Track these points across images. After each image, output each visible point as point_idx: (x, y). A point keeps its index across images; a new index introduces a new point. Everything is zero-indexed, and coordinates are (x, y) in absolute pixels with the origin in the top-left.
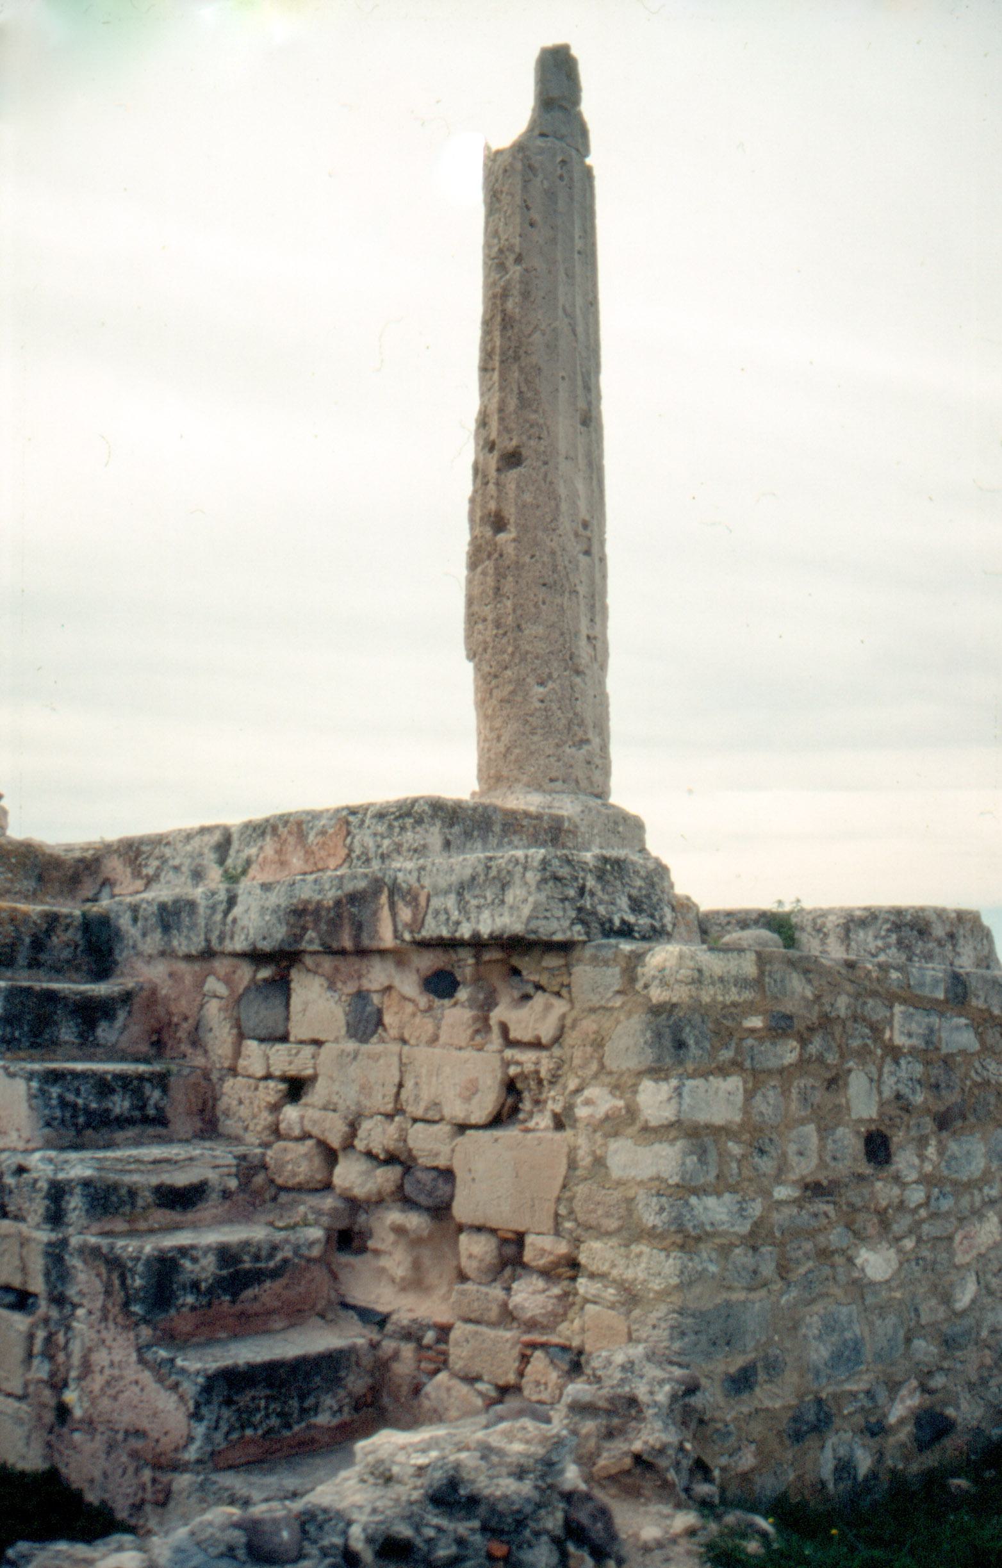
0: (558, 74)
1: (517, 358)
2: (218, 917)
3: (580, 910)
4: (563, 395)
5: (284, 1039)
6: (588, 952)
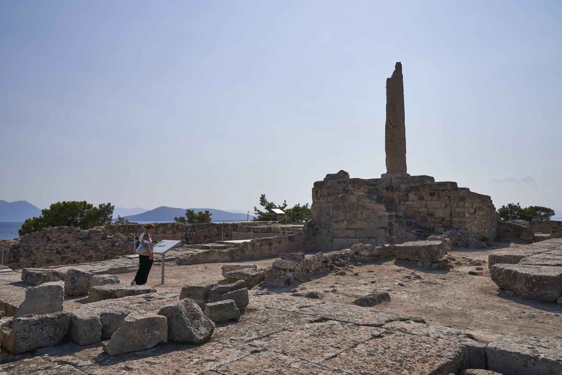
0: (399, 66)
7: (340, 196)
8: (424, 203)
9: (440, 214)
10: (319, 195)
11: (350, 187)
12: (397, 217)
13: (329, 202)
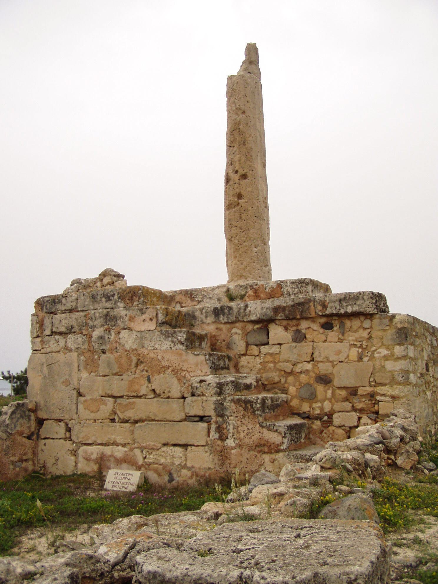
0: (252, 53)
1: (244, 145)
2: (242, 311)
3: (377, 306)
4: (259, 158)
5: (267, 344)
6: (377, 316)
7: (97, 333)
8: (306, 348)
9: (344, 377)
10: (48, 332)
11: (121, 310)
12: (237, 386)
13: (70, 350)
